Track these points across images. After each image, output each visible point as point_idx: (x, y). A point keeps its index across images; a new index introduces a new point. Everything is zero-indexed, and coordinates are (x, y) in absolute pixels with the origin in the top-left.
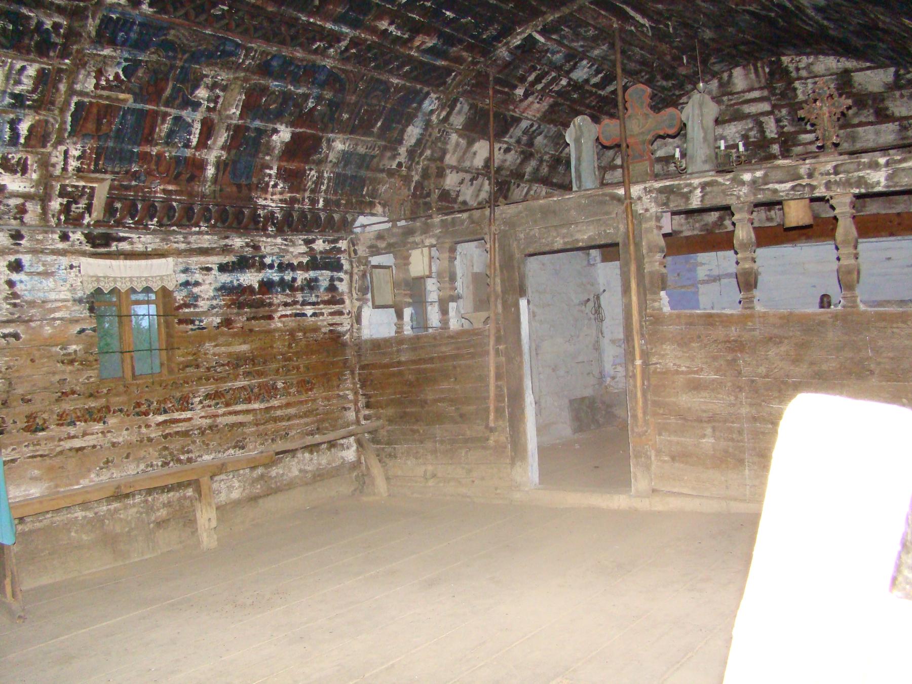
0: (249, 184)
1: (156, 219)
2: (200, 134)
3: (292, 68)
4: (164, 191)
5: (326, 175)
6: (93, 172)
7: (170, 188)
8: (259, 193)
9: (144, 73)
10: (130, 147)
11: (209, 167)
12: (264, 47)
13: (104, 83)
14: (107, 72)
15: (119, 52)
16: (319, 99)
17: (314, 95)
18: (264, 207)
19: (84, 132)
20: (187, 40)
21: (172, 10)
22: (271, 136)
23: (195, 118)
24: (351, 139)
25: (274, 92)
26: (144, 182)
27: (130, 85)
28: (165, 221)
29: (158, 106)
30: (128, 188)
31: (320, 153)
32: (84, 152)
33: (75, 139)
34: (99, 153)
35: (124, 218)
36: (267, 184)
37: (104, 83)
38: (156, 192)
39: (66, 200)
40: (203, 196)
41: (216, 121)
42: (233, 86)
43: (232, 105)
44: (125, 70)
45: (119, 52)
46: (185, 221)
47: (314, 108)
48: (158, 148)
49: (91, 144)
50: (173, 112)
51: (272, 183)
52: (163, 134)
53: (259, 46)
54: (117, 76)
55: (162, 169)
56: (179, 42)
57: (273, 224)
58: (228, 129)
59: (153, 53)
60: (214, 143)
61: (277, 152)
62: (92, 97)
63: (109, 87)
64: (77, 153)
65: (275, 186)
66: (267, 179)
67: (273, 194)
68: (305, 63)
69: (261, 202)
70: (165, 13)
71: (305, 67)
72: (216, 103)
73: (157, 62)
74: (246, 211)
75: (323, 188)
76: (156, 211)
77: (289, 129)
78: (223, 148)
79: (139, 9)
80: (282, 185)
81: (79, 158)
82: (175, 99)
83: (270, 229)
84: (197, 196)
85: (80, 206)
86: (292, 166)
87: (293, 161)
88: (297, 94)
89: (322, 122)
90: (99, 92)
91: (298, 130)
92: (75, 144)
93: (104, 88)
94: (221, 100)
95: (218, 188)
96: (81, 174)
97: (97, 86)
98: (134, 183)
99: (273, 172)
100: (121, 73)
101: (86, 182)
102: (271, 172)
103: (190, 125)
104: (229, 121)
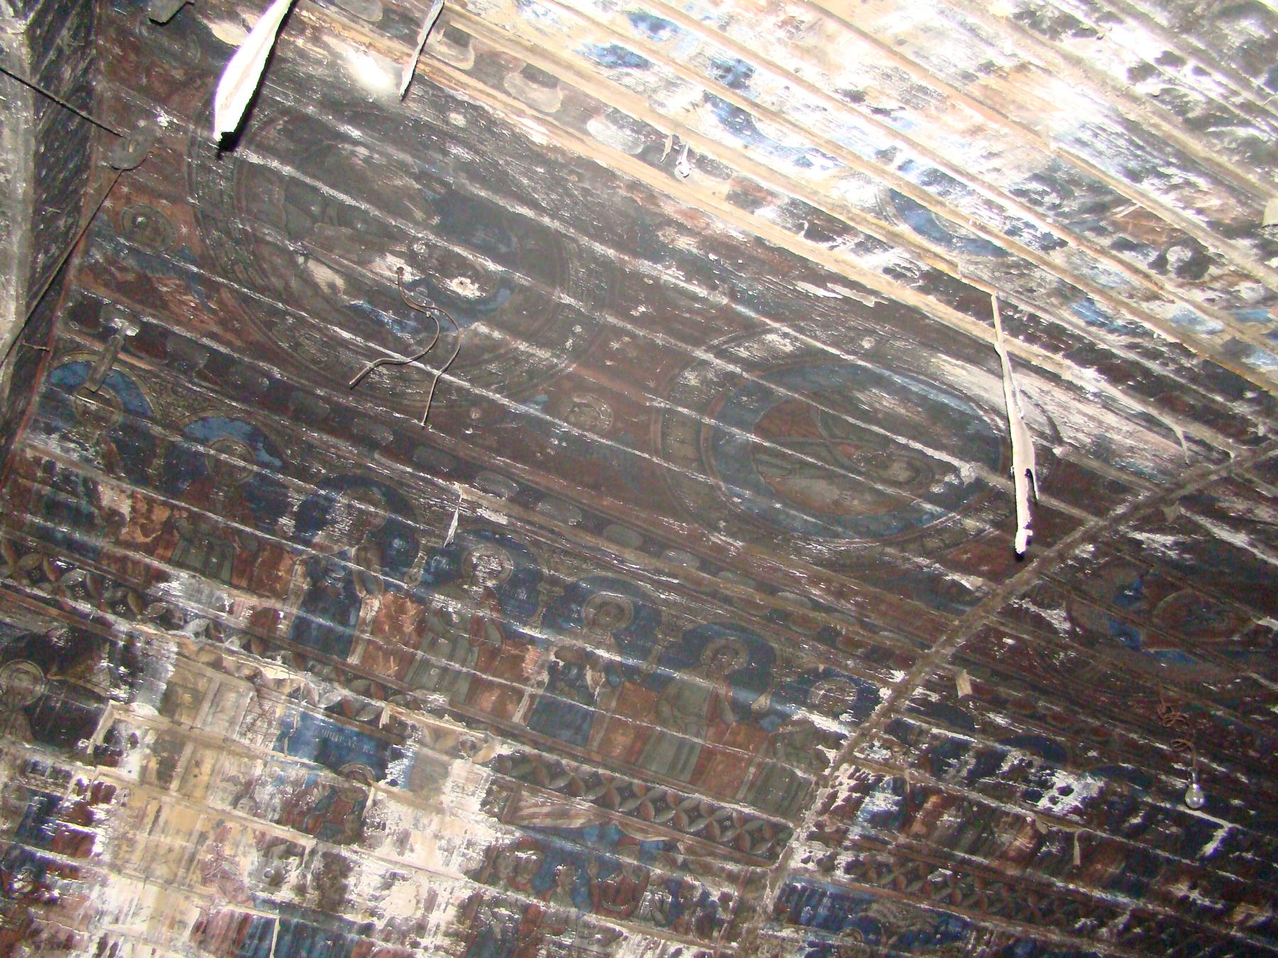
21: (875, 876)
53: (997, 926)
59: (848, 935)
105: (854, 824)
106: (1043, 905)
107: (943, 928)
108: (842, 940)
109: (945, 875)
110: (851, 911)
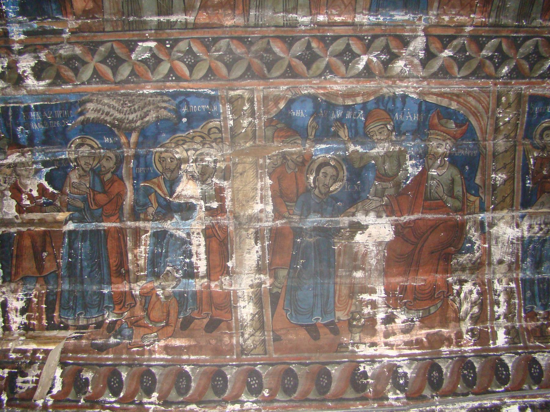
0: (332, 323)
1: (155, 395)
2: (208, 252)
3: (339, 114)
4: (167, 349)
5: (498, 287)
6: (48, 329)
7: (177, 342)
8: (357, 337)
9: (80, 176)
10: (95, 288)
11: (241, 304)
12: (260, 90)
13: (28, 202)
14: (26, 186)
15: (29, 155)
16: (424, 156)
17: (412, 151)
18: (372, 360)
19: (21, 275)
20: (120, 112)
21: (71, 74)
22: (352, 236)
23: (193, 230)
24: (531, 216)
25: (325, 164)
26: (130, 337)
27: (66, 198)
28: (173, 395)
29: (121, 221)
30: (102, 349)
31: (470, 250)
32: (29, 302)
33: (13, 286)
34: (51, 301)
35: (101, 394)
36: (372, 320)
37: (28, 202)
38: (151, 352)
39: (7, 371)
40: (243, 351)
41: (231, 228)
42: (240, 168)
43: (253, 198)
44: (49, 178)
45: (29, 155)
46: (210, 395)
47: (423, 176)
48: (142, 283)
49: (36, 290)
50: (150, 226)
51: (381, 316)
52: (142, 262)
53: (252, 91)
54: (42, 189)
55: (156, 314)
56: (108, 119)
57: (397, 387)
58: (258, 236)
59: (81, 145)
60: (240, 263)
61: (373, 262)
62: (19, 225)
63: (37, 208)
64: (20, 305)
65: (390, 319)
66: (367, 310)
67: (387, 335)
68: (359, 100)
69: (364, 350)
70: (66, 82)
71: (364, 105)
72: (221, 199)
73: (92, 156)
74: (334, 370)
75: (501, 310)
76: (154, 381)
77: (385, 220)
78: (259, 269)
79: (25, 87)
80: (404, 317)
81: (23, 311)
82: (145, 206)
83: (391, 395)
84: (230, 351)
85: (29, 378)
86: (419, 281)
87: (416, 272)
88: (374, 158)
89: (452, 196)
90: (27, 216)
91: (406, 218)
92: (14, 291)
93: (30, 210)
94: (228, 194)
95: (269, 336)
96: (31, 333)
97: (20, 209)
98: (112, 340)
99: (379, 296)
100: (46, 184)
101: (39, 343)
102: (374, 297)
103: (185, 242)
104: (258, 225)
105: (7, 23)
106: (298, 48)
107: (184, 110)
108: (76, 152)
109: (151, 49)
110: (67, 118)
